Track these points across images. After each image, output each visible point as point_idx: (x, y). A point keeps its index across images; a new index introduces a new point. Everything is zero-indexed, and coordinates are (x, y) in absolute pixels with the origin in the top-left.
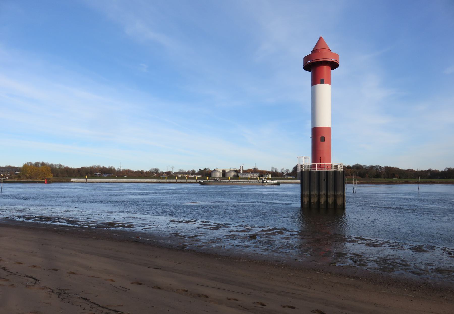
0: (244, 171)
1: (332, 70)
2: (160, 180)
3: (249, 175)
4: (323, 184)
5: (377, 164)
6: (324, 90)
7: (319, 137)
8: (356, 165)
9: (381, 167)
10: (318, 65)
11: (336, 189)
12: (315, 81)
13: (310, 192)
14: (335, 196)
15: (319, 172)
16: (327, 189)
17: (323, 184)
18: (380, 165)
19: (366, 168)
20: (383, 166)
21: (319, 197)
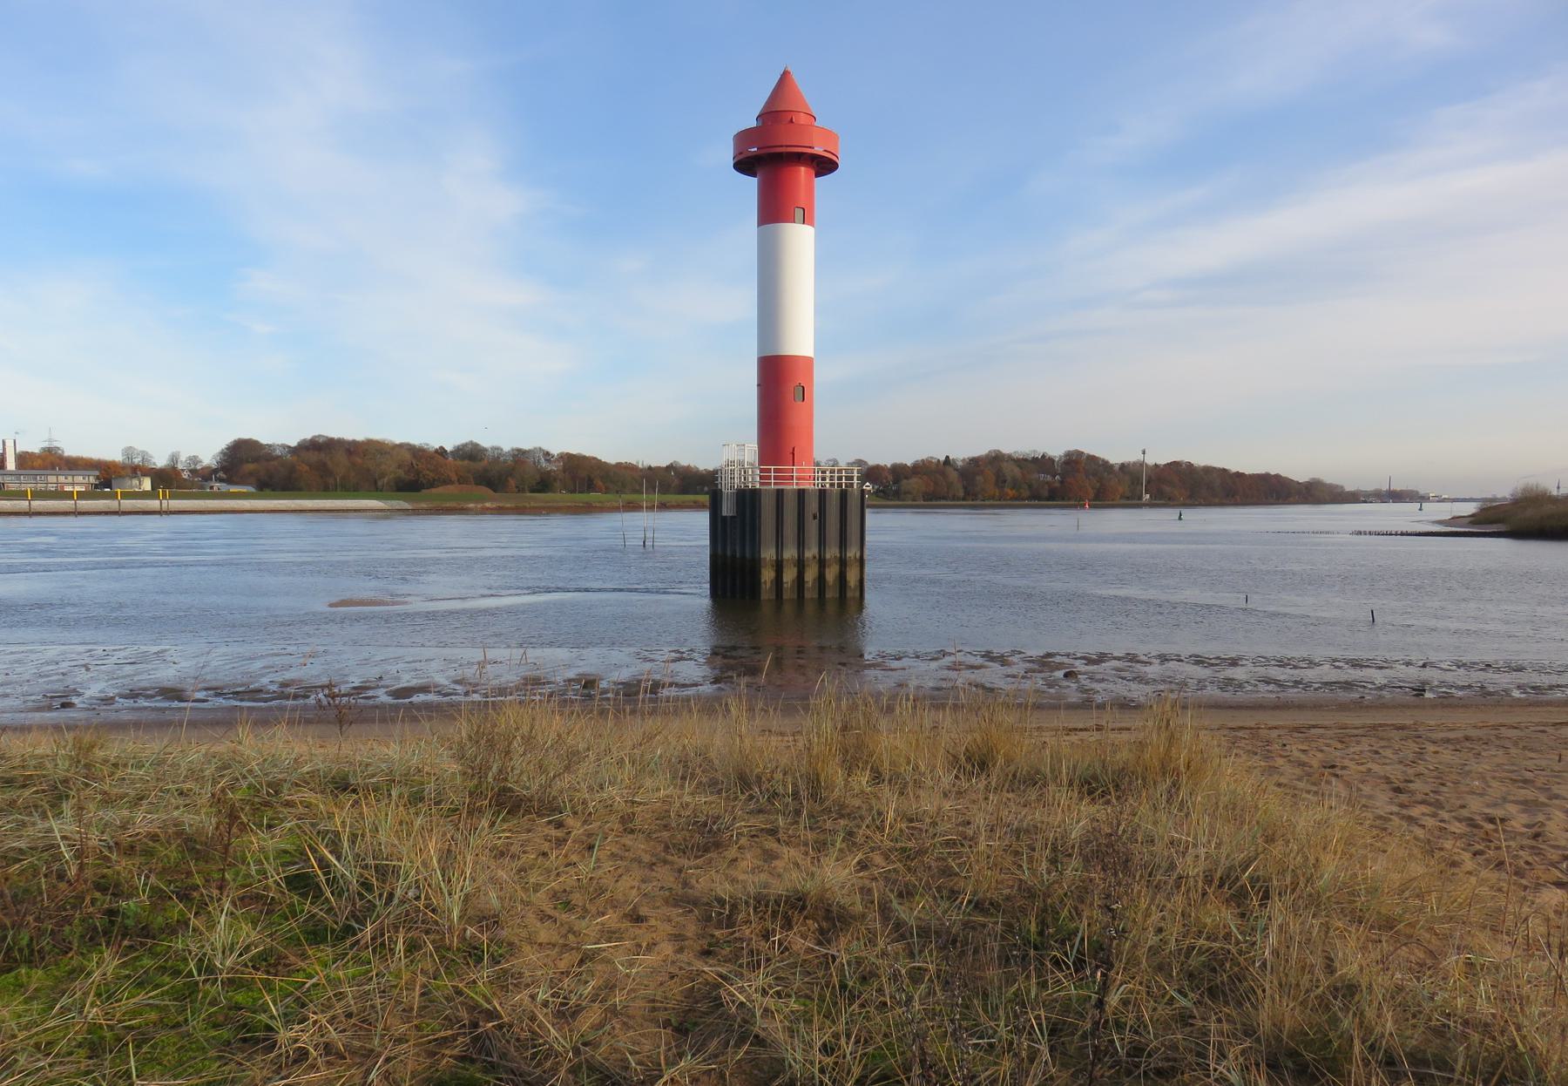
0: (24, 460)
2: (111, 504)
3: (52, 481)
4: (812, 527)
5: (537, 445)
6: (800, 239)
7: (779, 380)
9: (548, 453)
11: (843, 543)
12: (774, 209)
14: (843, 563)
15: (780, 494)
16: (822, 543)
17: (812, 527)
18: (546, 448)
20: (555, 450)
21: (801, 564)
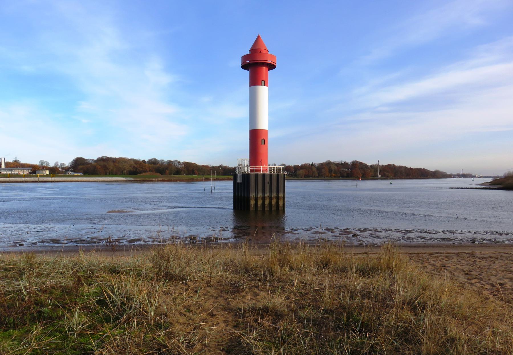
1: (269, 70)
3: (17, 171)
4: (267, 186)
5: (176, 159)
6: (263, 91)
7: (256, 138)
8: (152, 159)
9: (179, 162)
10: (256, 65)
11: (278, 192)
13: (256, 195)
14: (278, 198)
17: (267, 186)
18: (179, 160)
19: (163, 163)
20: (182, 161)
